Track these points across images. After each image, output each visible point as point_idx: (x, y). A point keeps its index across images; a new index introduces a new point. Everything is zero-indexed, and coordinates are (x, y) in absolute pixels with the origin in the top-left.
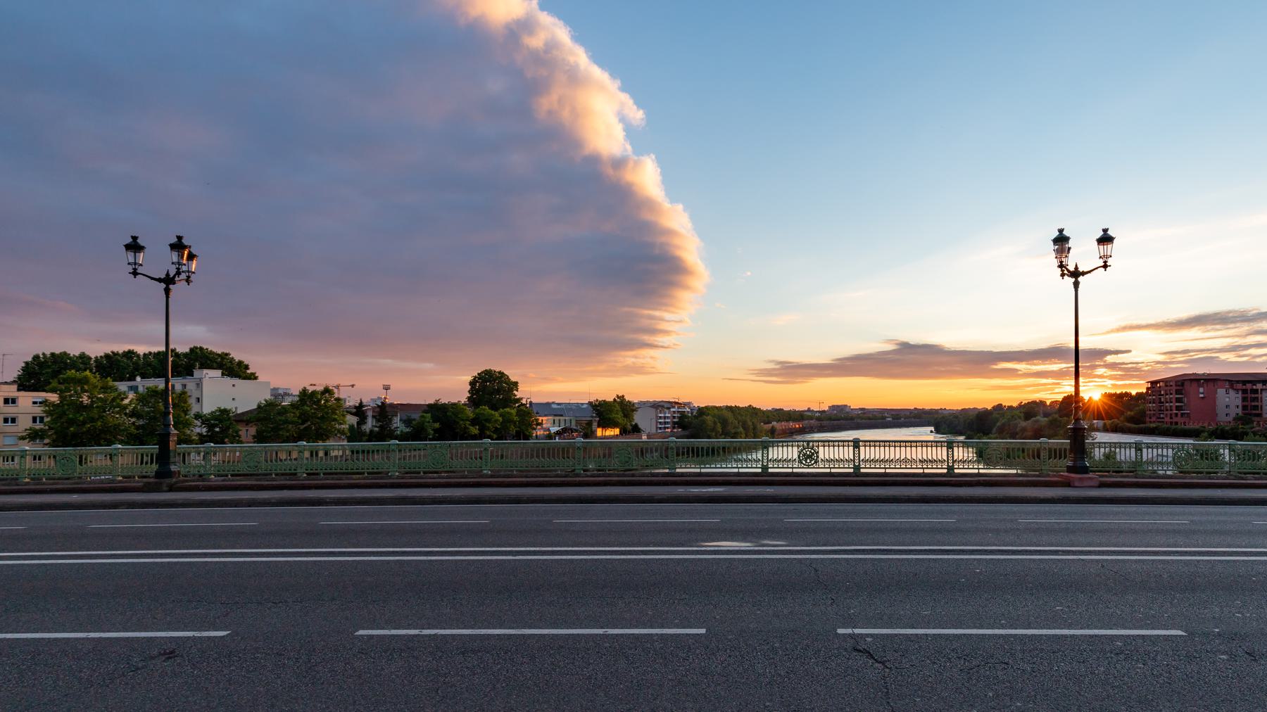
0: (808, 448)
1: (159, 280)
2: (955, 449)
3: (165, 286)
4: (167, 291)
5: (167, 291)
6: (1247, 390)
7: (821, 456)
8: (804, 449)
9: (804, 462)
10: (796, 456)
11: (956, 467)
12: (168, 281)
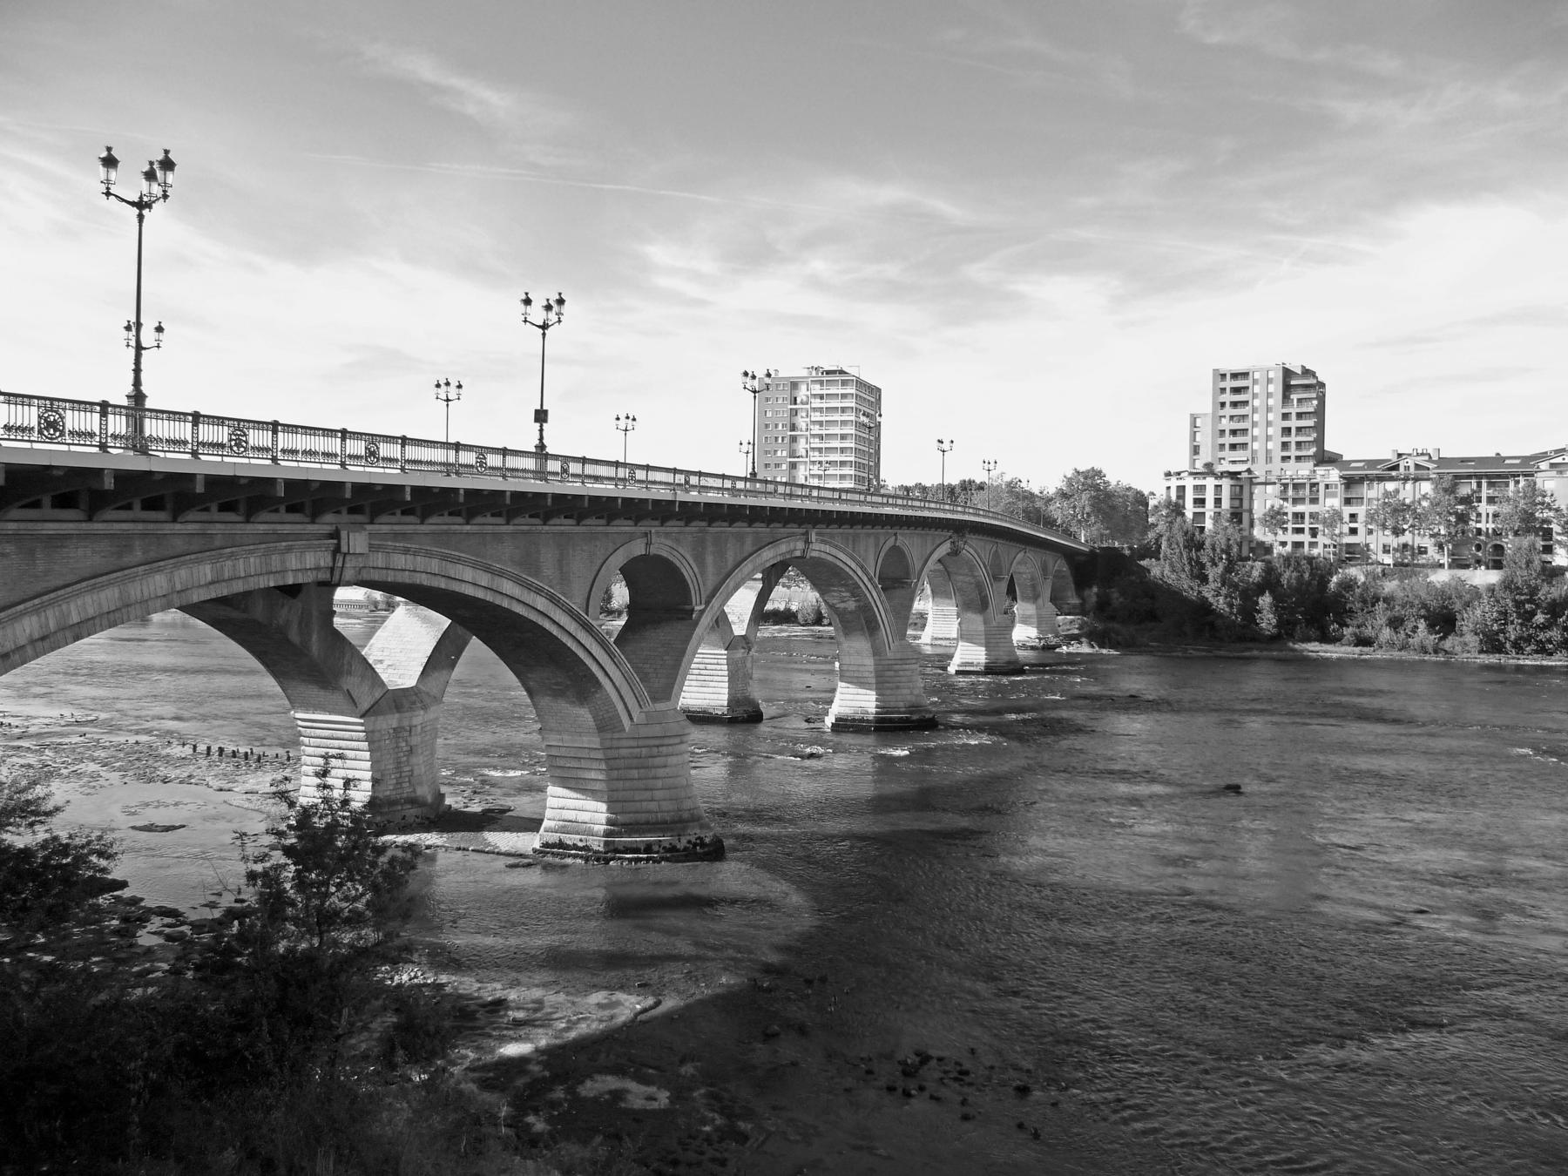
0: (52, 411)
1: (539, 327)
2: (201, 426)
3: (138, 211)
4: (141, 217)
5: (141, 217)
6: (1466, 523)
7: (69, 426)
8: (47, 411)
9: (46, 433)
10: (34, 423)
11: (200, 451)
12: (544, 327)
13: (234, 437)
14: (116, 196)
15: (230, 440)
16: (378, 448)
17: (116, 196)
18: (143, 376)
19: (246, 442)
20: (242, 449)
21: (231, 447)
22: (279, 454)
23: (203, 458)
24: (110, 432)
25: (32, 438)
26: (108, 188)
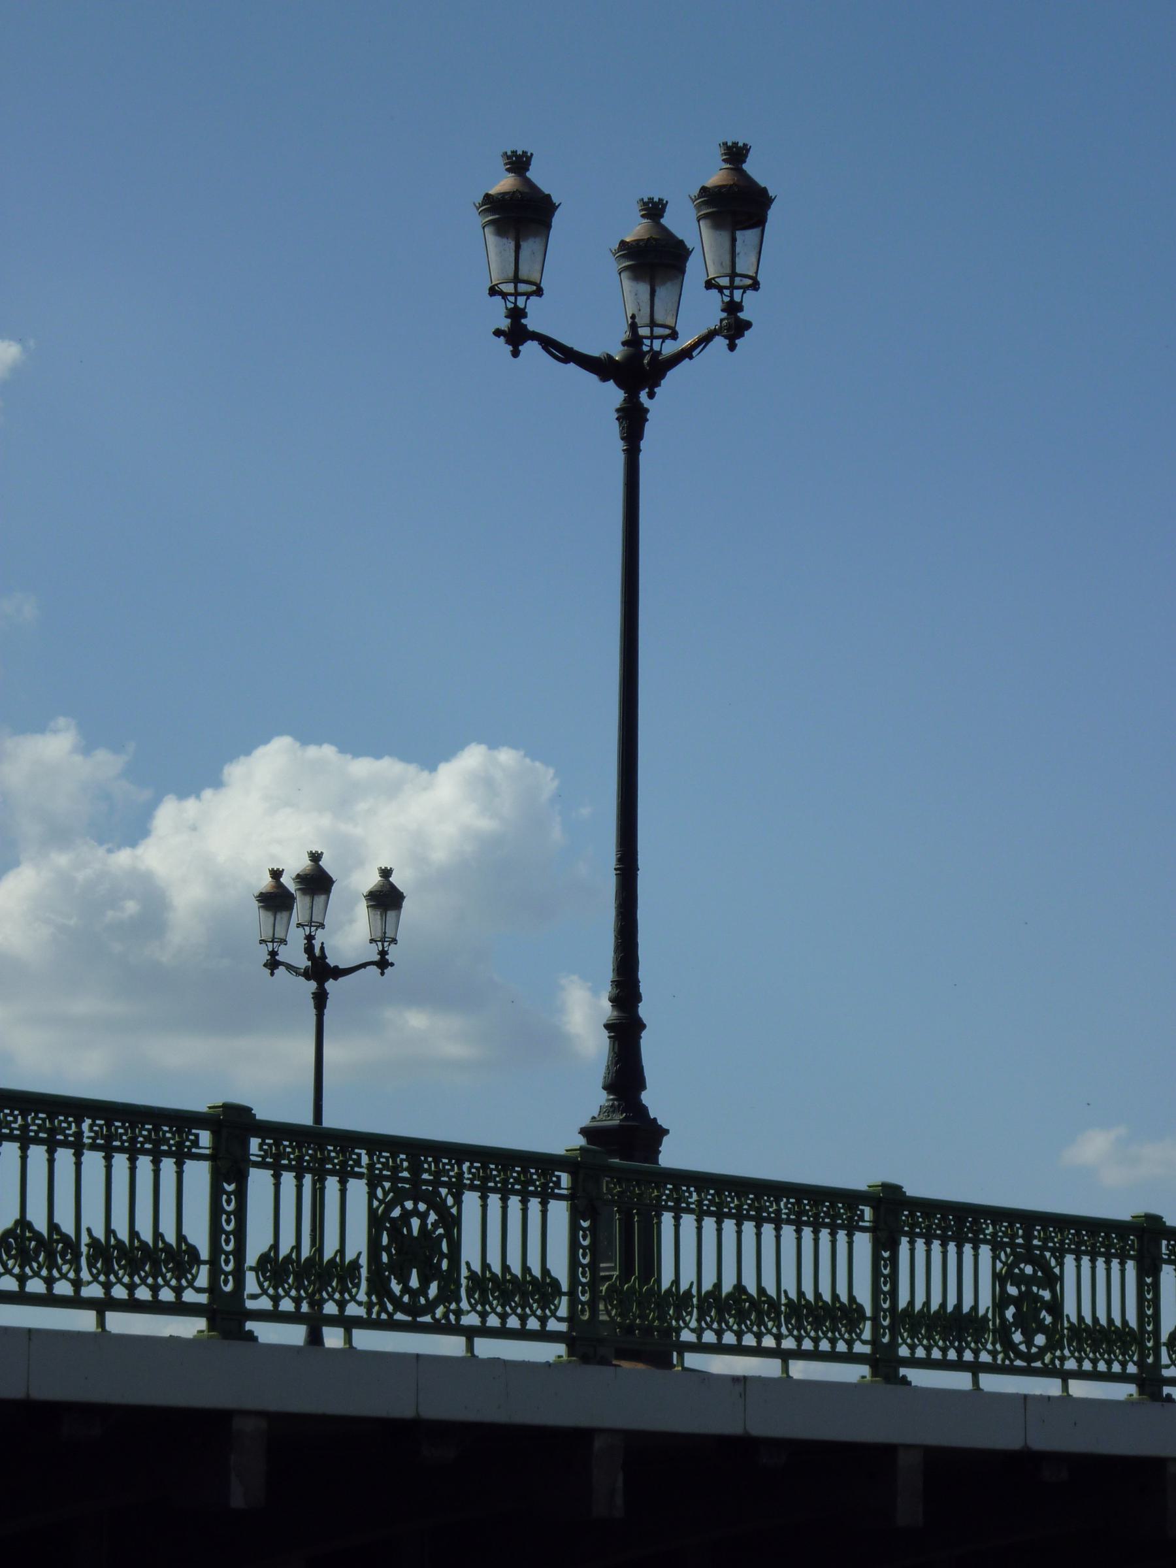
1: (601, 367)
8: (398, 1200)
11: (904, 1351)
13: (1012, 1290)
14: (548, 344)
15: (1000, 1302)
16: (452, 1223)
17: (548, 344)
18: (649, 1044)
19: (1055, 1307)
20: (1040, 1340)
21: (1004, 1334)
22: (251, 1284)
23: (918, 1377)
24: (257, 1244)
25: (352, 1310)
26: (517, 314)
